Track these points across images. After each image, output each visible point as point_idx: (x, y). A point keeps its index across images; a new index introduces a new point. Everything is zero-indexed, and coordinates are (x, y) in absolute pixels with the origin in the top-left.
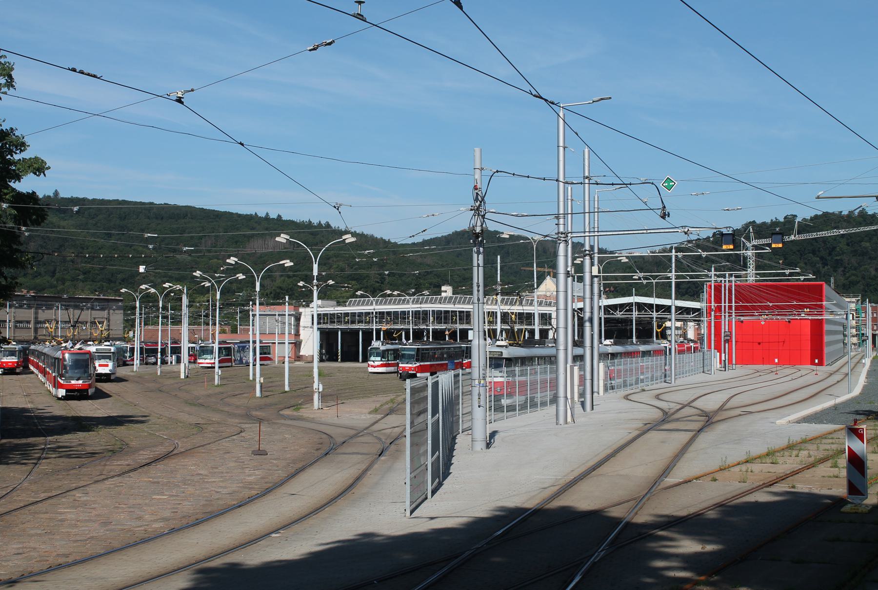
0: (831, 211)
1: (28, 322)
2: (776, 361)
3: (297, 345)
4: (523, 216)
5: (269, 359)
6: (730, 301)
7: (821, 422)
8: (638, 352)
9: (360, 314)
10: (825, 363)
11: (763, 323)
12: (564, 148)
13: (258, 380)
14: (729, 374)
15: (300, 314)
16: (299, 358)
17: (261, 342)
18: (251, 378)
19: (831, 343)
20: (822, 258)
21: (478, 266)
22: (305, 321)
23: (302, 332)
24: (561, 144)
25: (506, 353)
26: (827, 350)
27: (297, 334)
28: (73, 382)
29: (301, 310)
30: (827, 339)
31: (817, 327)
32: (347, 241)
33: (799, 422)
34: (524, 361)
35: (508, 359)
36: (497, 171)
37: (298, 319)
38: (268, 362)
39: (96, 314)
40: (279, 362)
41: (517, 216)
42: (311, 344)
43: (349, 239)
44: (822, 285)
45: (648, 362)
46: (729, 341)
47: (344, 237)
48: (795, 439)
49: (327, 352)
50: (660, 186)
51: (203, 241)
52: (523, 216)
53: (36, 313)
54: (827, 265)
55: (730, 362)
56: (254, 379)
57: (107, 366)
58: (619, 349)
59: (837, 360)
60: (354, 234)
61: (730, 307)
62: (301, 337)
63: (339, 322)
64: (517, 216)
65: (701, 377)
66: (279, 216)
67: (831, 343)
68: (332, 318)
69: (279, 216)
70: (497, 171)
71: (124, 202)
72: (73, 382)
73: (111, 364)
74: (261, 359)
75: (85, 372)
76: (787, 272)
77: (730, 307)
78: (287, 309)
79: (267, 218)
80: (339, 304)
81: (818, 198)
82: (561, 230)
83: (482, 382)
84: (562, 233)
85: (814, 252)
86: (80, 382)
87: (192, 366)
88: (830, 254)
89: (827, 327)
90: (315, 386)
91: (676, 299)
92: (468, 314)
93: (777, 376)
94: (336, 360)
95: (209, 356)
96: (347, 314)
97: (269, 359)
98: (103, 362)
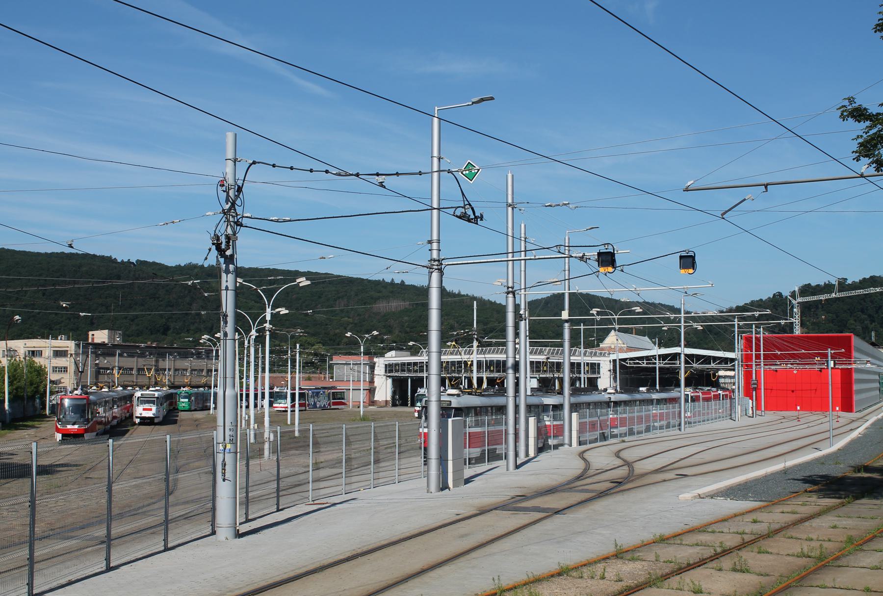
0: (878, 275)
1: (132, 369)
2: (798, 408)
3: (371, 391)
4: (285, 221)
5: (344, 404)
6: (758, 349)
7: (745, 498)
8: (635, 401)
9: (409, 364)
10: (855, 410)
11: (795, 372)
12: (439, 159)
13: (252, 427)
14: (757, 420)
15: (375, 364)
16: (372, 403)
17: (300, 389)
18: (289, 423)
19: (860, 391)
20: (870, 316)
21: (227, 289)
22: (380, 370)
23: (376, 379)
24: (436, 154)
25: (455, 403)
26: (856, 398)
27: (372, 381)
28: (69, 427)
29: (375, 360)
30: (856, 387)
31: (847, 377)
32: (301, 285)
33: (712, 496)
34: (626, 403)
35: (456, 409)
36: (254, 163)
37: (372, 367)
38: (343, 407)
39: (141, 362)
40: (353, 406)
41: (277, 221)
42: (384, 390)
43: (303, 282)
44: (850, 337)
45: (655, 410)
46: (757, 389)
47: (298, 281)
48: (568, 563)
49: (400, 398)
50: (459, 175)
51: (337, 302)
52: (285, 221)
53: (157, 361)
54: (874, 321)
55: (758, 407)
56: (293, 424)
57: (151, 410)
58: (624, 397)
59: (875, 404)
60: (308, 275)
61: (758, 357)
62: (376, 384)
63: (409, 371)
64: (277, 221)
65: (728, 423)
66: (402, 281)
67: (860, 391)
68: (404, 366)
69: (402, 281)
70: (254, 163)
71: (339, 276)
72: (69, 427)
73: (154, 408)
74: (300, 405)
75: (82, 417)
76: (757, 314)
77: (758, 357)
78: (363, 359)
79: (392, 283)
80: (413, 354)
81: (687, 190)
82: (435, 256)
83: (229, 446)
84: (435, 261)
85: (862, 311)
86: (76, 427)
87: (272, 410)
88: (877, 312)
89: (855, 376)
90: (266, 435)
91: (686, 346)
92: (572, 365)
93: (799, 423)
94: (407, 405)
95: (283, 401)
96: (415, 364)
97: (344, 404)
98: (147, 406)
